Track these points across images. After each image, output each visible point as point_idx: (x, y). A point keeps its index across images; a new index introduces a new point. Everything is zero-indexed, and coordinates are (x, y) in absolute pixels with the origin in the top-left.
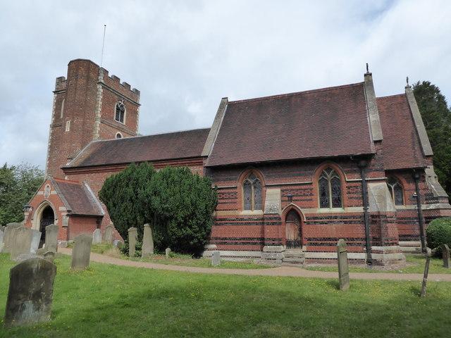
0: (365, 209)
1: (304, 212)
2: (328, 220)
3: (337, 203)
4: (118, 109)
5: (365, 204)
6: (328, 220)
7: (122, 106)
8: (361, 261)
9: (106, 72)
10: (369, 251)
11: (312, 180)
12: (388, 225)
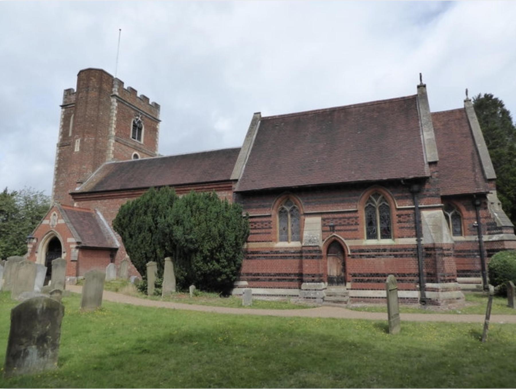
0: (419, 241)
1: (349, 244)
2: (376, 253)
3: (386, 234)
4: (135, 126)
5: (418, 235)
6: (376, 253)
7: (139, 122)
8: (413, 300)
9: (121, 83)
10: (422, 289)
11: (357, 207)
12: (445, 259)
